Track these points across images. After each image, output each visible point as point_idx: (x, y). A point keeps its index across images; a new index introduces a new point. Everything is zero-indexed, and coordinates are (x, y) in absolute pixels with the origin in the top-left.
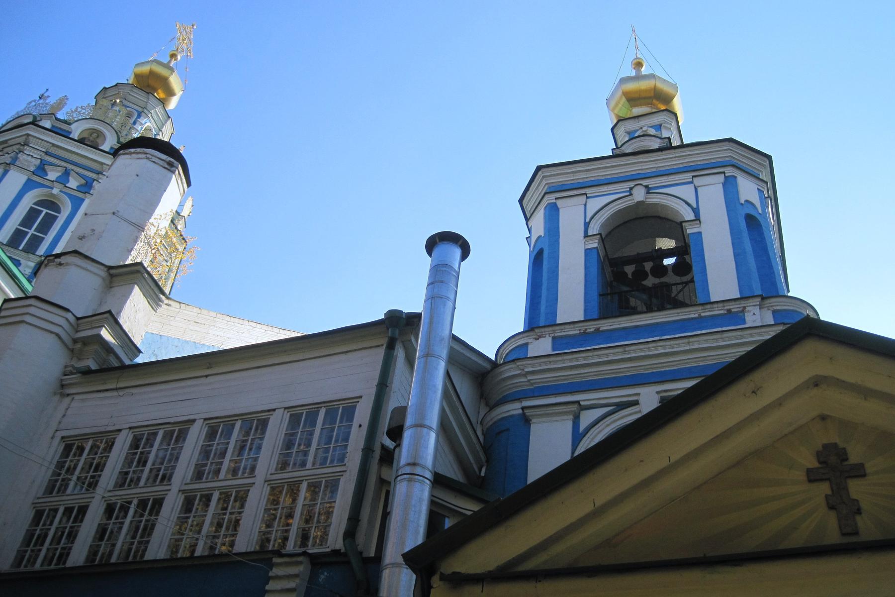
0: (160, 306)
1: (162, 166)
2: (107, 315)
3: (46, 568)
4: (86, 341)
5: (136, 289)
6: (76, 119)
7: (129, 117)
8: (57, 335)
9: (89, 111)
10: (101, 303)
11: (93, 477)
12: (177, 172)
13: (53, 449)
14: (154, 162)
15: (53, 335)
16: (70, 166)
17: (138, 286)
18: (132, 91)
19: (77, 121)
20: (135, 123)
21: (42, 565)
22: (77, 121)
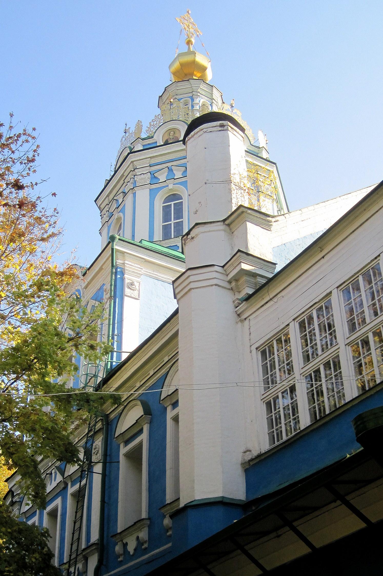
0: (272, 225)
1: (217, 131)
2: (239, 253)
3: (290, 436)
4: (236, 279)
5: (249, 225)
6: (154, 131)
7: (187, 105)
8: (216, 285)
9: (159, 120)
10: (232, 247)
11: (288, 364)
12: (229, 128)
13: (255, 360)
14: (211, 132)
15: (214, 287)
16: (169, 165)
17: (248, 221)
18: (178, 86)
19: (155, 132)
20: (193, 106)
21: (287, 435)
22: (155, 132)
